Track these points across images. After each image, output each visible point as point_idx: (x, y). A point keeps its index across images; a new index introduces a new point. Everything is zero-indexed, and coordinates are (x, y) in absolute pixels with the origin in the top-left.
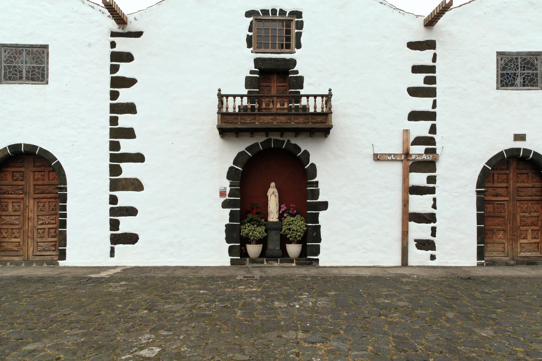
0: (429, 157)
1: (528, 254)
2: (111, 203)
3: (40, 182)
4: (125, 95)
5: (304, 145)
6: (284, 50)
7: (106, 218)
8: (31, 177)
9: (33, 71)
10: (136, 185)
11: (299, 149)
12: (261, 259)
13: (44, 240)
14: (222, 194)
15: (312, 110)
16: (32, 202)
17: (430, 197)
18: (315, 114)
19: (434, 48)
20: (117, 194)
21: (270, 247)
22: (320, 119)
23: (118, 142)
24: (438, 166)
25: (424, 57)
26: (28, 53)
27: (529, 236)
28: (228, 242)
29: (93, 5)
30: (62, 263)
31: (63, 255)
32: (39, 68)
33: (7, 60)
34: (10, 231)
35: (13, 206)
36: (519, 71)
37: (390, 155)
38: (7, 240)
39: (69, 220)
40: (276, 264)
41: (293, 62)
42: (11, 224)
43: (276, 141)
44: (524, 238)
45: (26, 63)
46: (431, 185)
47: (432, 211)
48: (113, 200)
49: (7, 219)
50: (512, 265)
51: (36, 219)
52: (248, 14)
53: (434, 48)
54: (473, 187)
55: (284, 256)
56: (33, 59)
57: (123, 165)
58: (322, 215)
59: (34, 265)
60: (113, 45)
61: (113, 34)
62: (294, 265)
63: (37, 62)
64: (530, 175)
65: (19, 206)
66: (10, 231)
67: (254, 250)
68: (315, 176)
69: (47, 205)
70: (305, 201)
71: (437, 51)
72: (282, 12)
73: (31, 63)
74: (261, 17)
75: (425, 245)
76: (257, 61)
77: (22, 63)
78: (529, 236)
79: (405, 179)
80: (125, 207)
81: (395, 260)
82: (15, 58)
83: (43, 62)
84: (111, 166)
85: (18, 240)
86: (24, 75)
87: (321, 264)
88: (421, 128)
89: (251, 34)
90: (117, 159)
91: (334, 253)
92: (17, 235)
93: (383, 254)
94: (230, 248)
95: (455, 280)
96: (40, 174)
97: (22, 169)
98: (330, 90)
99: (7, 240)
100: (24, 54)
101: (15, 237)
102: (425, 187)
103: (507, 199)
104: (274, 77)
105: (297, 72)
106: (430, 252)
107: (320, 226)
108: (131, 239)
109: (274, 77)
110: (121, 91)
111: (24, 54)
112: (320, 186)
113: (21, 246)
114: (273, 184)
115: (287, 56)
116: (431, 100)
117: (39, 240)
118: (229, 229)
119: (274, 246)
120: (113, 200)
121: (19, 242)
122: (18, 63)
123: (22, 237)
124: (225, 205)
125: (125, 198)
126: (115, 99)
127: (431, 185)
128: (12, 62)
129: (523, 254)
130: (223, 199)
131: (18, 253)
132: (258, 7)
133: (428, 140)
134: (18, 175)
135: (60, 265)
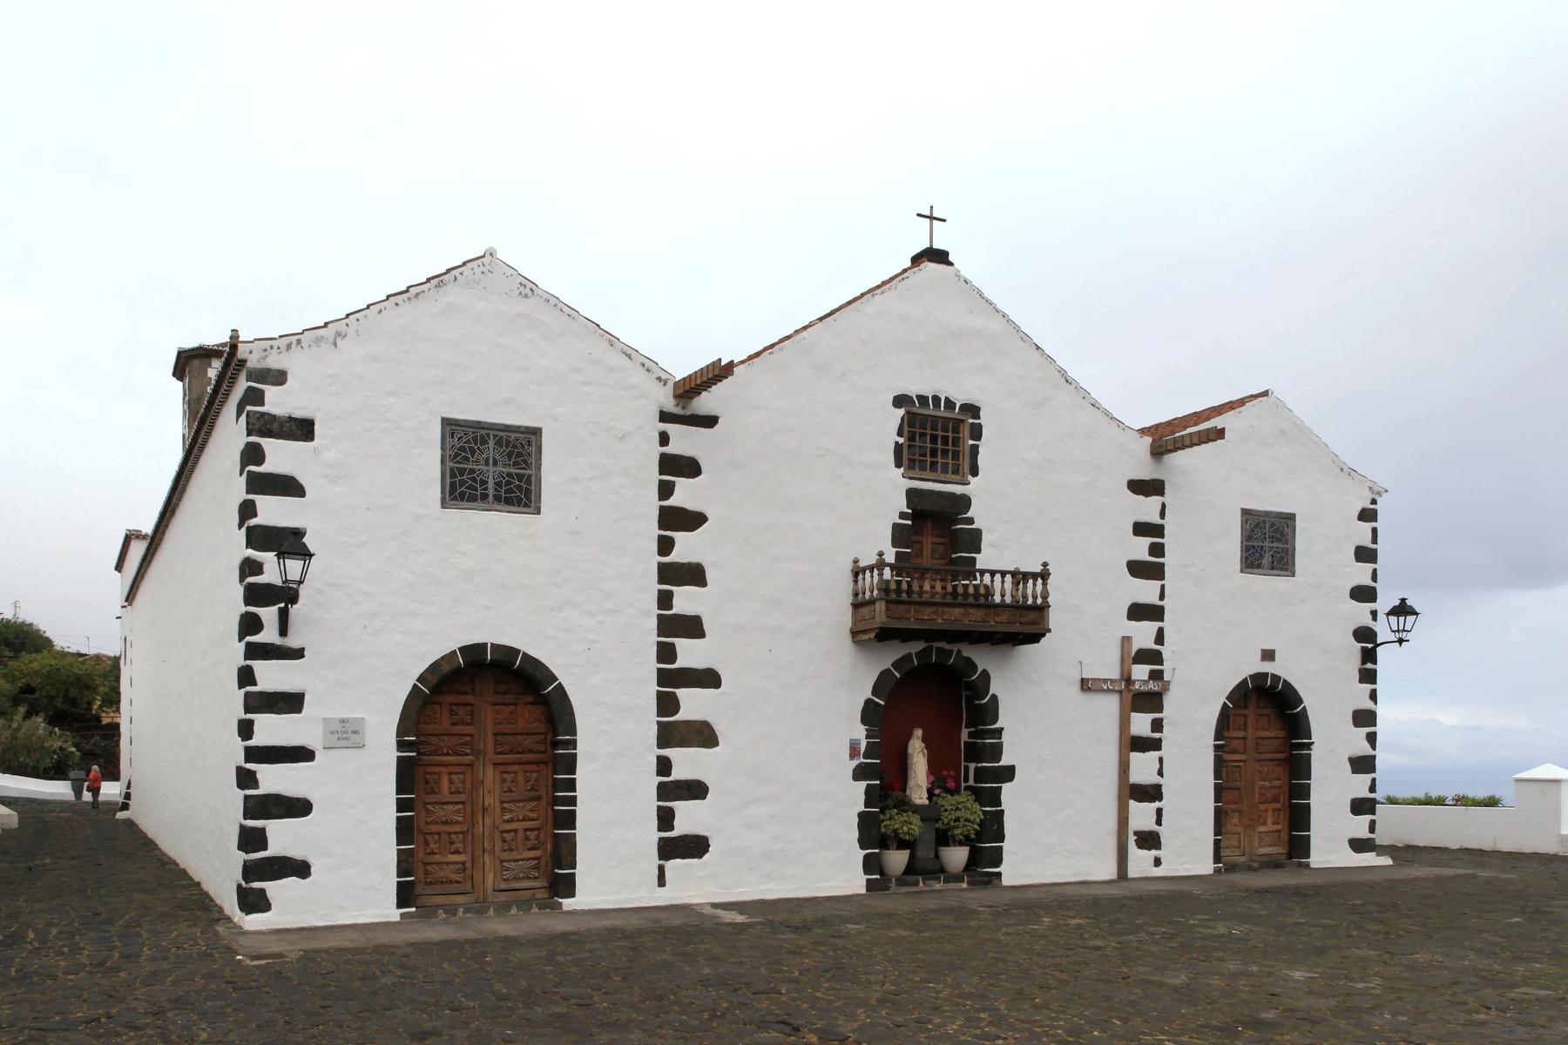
0: (1153, 686)
1: (1268, 850)
2: (659, 773)
3: (507, 728)
4: (687, 547)
5: (983, 658)
6: (950, 476)
7: (652, 803)
8: (527, 717)
9: (508, 483)
10: (703, 735)
11: (975, 667)
12: (912, 878)
13: (515, 855)
14: (854, 752)
15: (997, 599)
16: (490, 771)
17: (1154, 755)
18: (1003, 605)
19: (1162, 494)
20: (671, 753)
21: (920, 853)
22: (1032, 615)
23: (673, 645)
24: (1168, 701)
25: (1147, 508)
26: (499, 443)
27: (1270, 821)
28: (862, 847)
29: (629, 351)
30: (568, 904)
31: (567, 886)
32: (520, 477)
33: (457, 455)
34: (445, 838)
35: (451, 782)
36: (1267, 544)
37: (1105, 681)
38: (437, 858)
39: (581, 810)
40: (938, 886)
41: (965, 502)
42: (445, 823)
43: (940, 651)
44: (1264, 824)
45: (495, 463)
46: (1157, 735)
47: (1155, 779)
48: (664, 766)
49: (439, 812)
50: (1256, 870)
51: (498, 810)
52: (900, 401)
53: (1162, 494)
54: (1209, 740)
55: (937, 870)
56: (509, 455)
57: (683, 694)
58: (1006, 788)
59: (514, 911)
60: (664, 439)
61: (665, 417)
62: (965, 885)
63: (516, 464)
64: (1273, 717)
65: (464, 782)
66: (445, 838)
67: (897, 859)
68: (995, 720)
69: (521, 778)
70: (974, 762)
71: (1167, 499)
72: (950, 404)
73: (505, 465)
74: (917, 408)
75: (1149, 840)
76: (912, 494)
77: (487, 464)
78: (1270, 821)
79: (1124, 723)
80: (686, 782)
81: (1108, 871)
82: (473, 452)
83: (528, 465)
84: (660, 695)
85: (461, 858)
86: (491, 492)
87: (1006, 881)
88: (1143, 633)
89: (901, 440)
90: (673, 679)
91: (1026, 861)
92: (459, 846)
93: (1092, 863)
94: (866, 858)
95: (1173, 899)
96: (507, 709)
97: (470, 698)
98: (1045, 565)
99: (437, 858)
100: (491, 443)
101: (457, 852)
102: (1147, 739)
103: (1244, 757)
104: (936, 528)
105: (971, 521)
106: (1154, 852)
107: (1002, 812)
108: (695, 846)
109: (936, 528)
110: (680, 537)
111: (491, 443)
112: (1006, 738)
113: (469, 872)
114: (919, 732)
115: (958, 489)
116: (1157, 584)
117: (504, 856)
118: (865, 821)
119: (925, 852)
120: (664, 766)
121: (463, 863)
122: (477, 462)
123: (469, 850)
124: (859, 774)
125: (687, 763)
126: (667, 554)
127: (1157, 735)
128: (467, 459)
129: (1262, 851)
130: (855, 763)
131: (460, 888)
132: (913, 390)
133: (1150, 657)
134: (461, 711)
135: (565, 908)
